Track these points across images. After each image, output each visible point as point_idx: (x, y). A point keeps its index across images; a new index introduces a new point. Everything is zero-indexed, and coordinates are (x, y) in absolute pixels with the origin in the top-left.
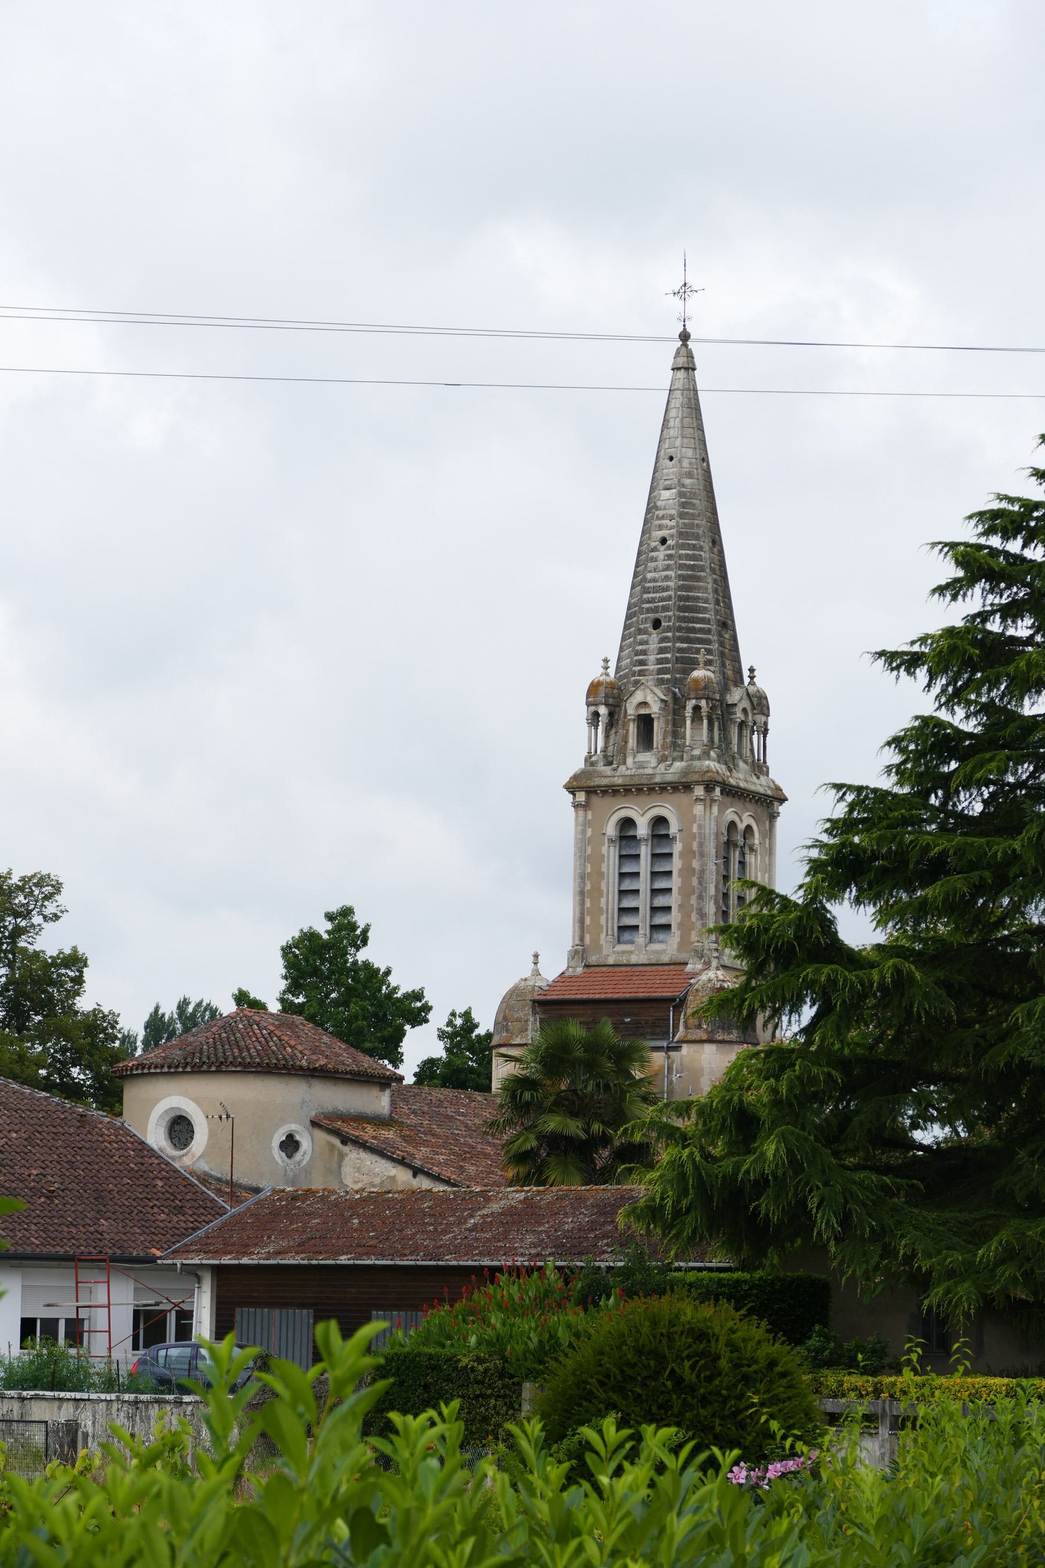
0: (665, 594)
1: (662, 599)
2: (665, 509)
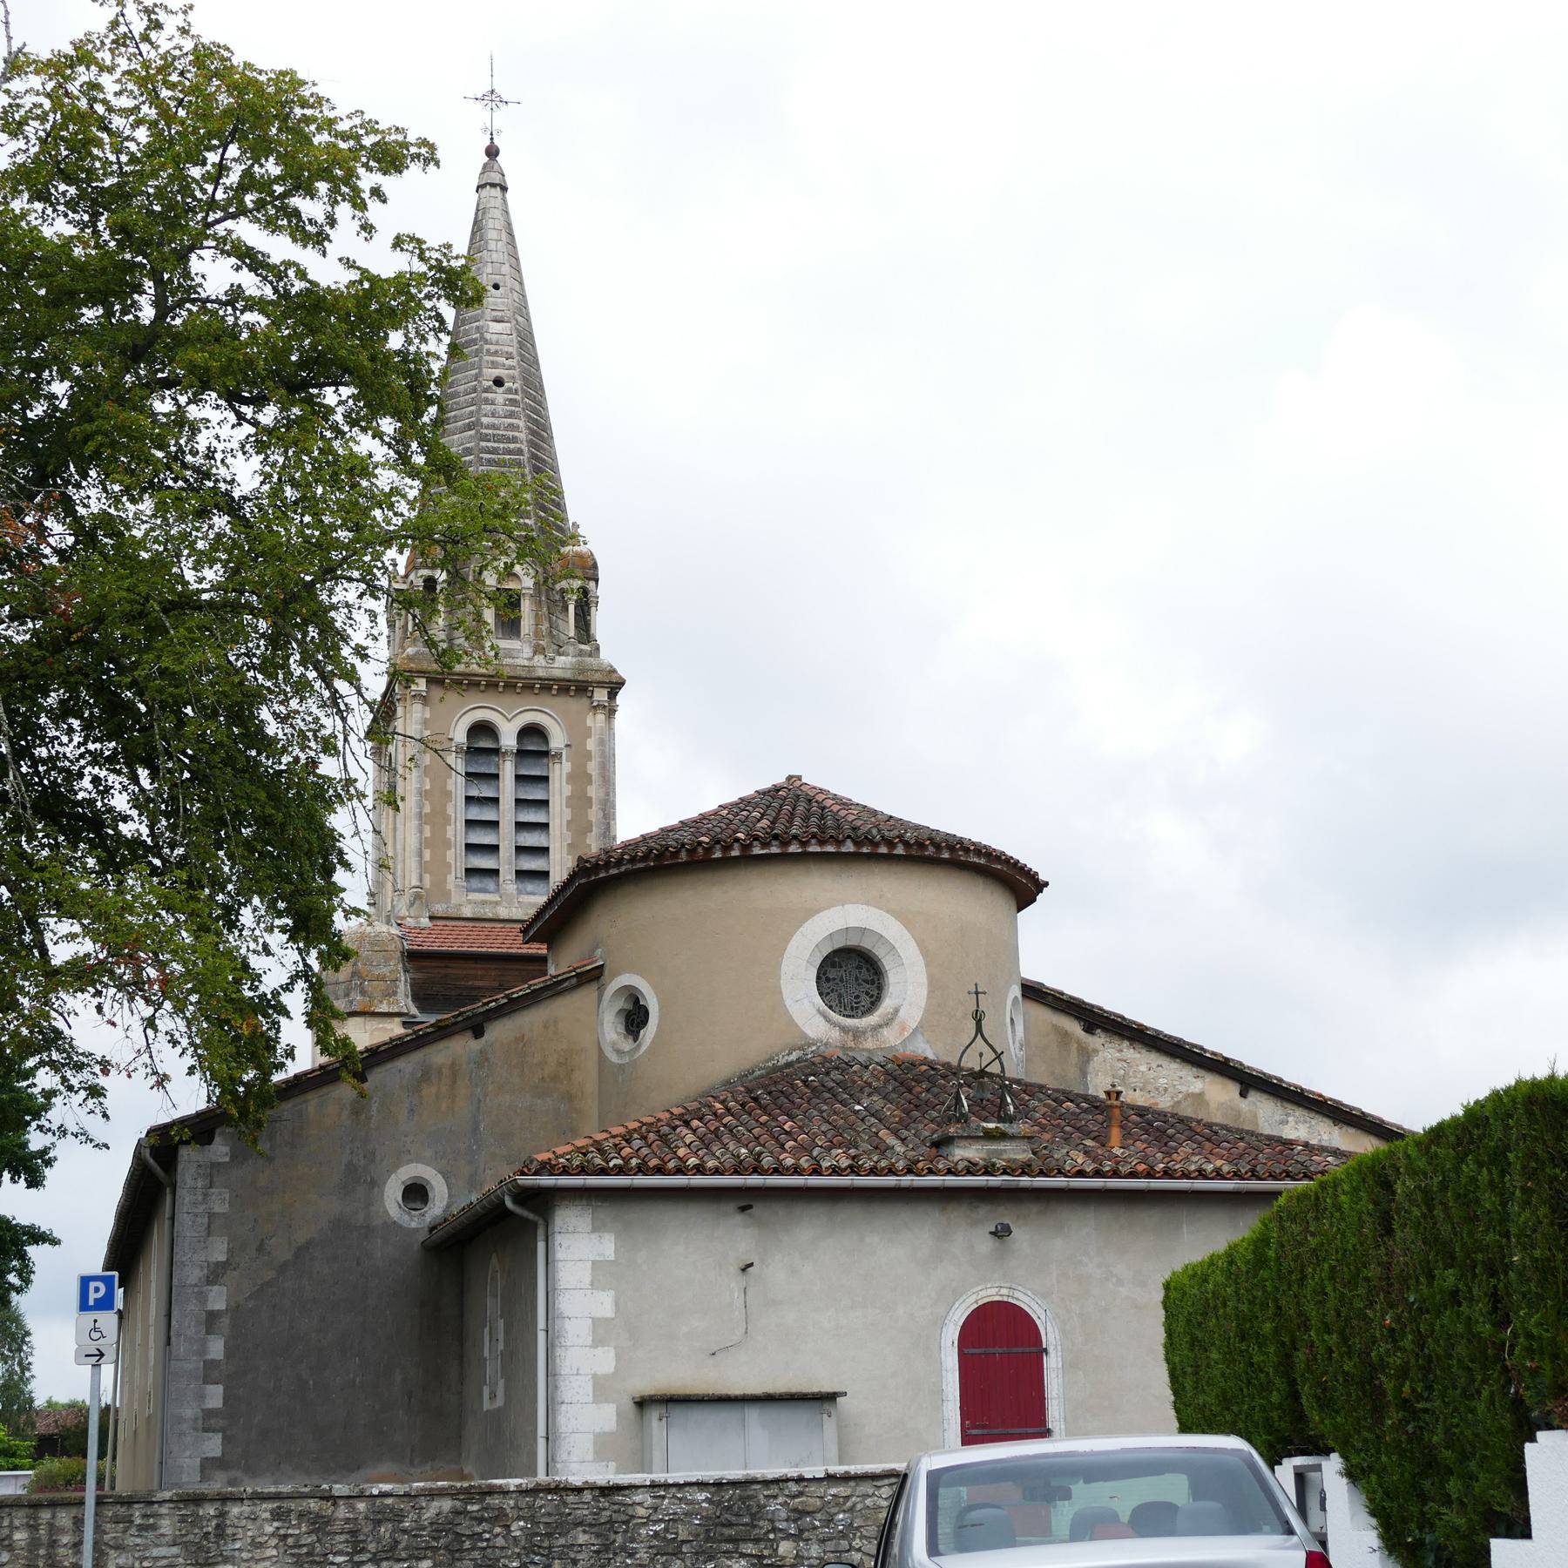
0: (512, 446)
1: (510, 452)
2: (497, 343)
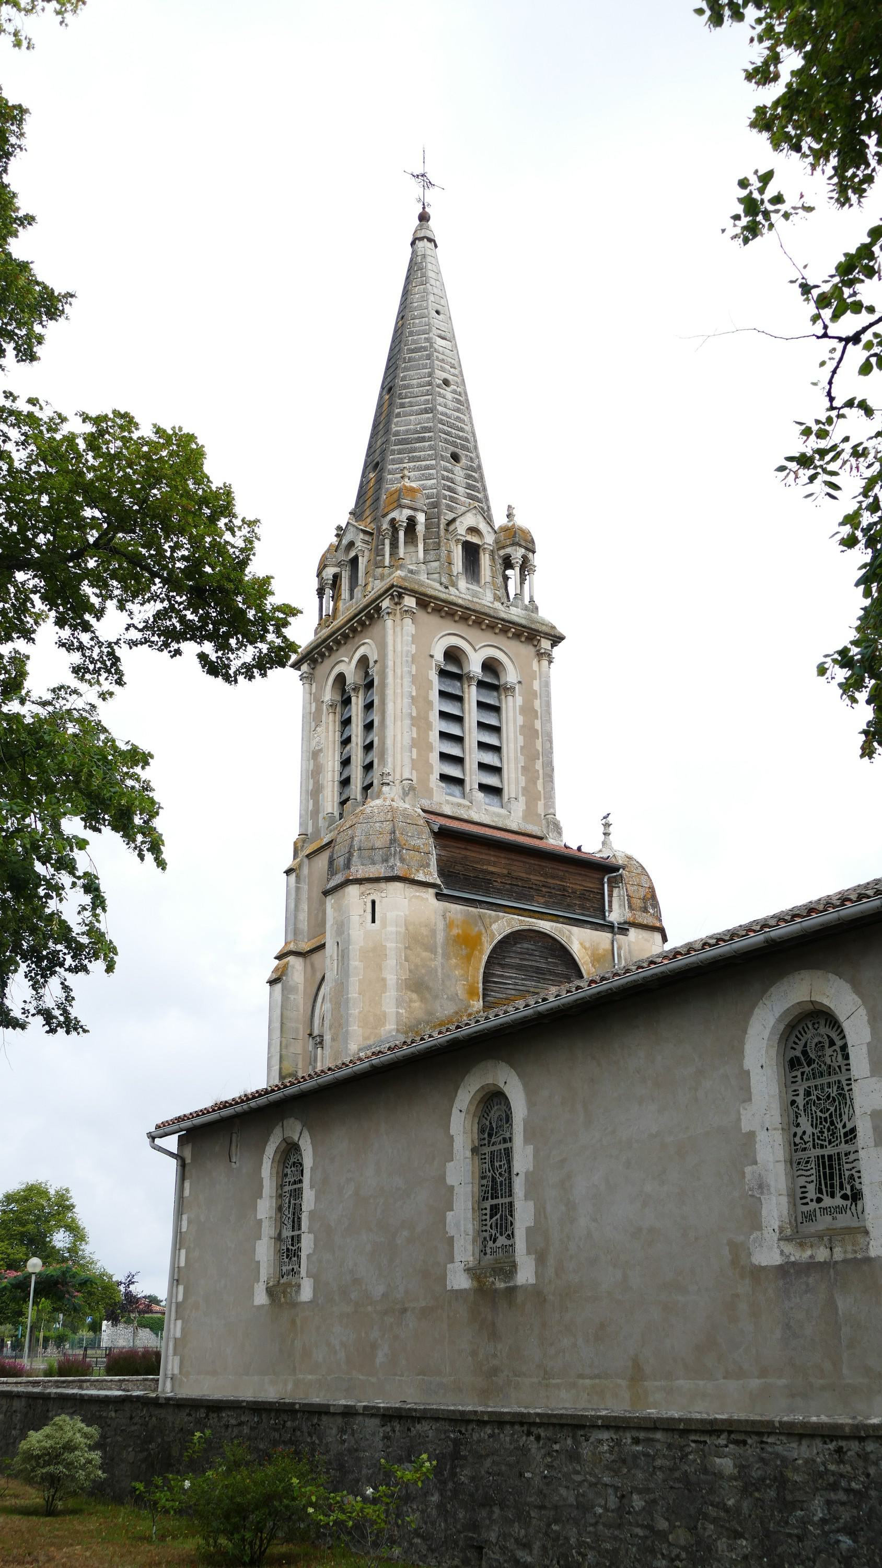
0: (461, 434)
1: (460, 438)
